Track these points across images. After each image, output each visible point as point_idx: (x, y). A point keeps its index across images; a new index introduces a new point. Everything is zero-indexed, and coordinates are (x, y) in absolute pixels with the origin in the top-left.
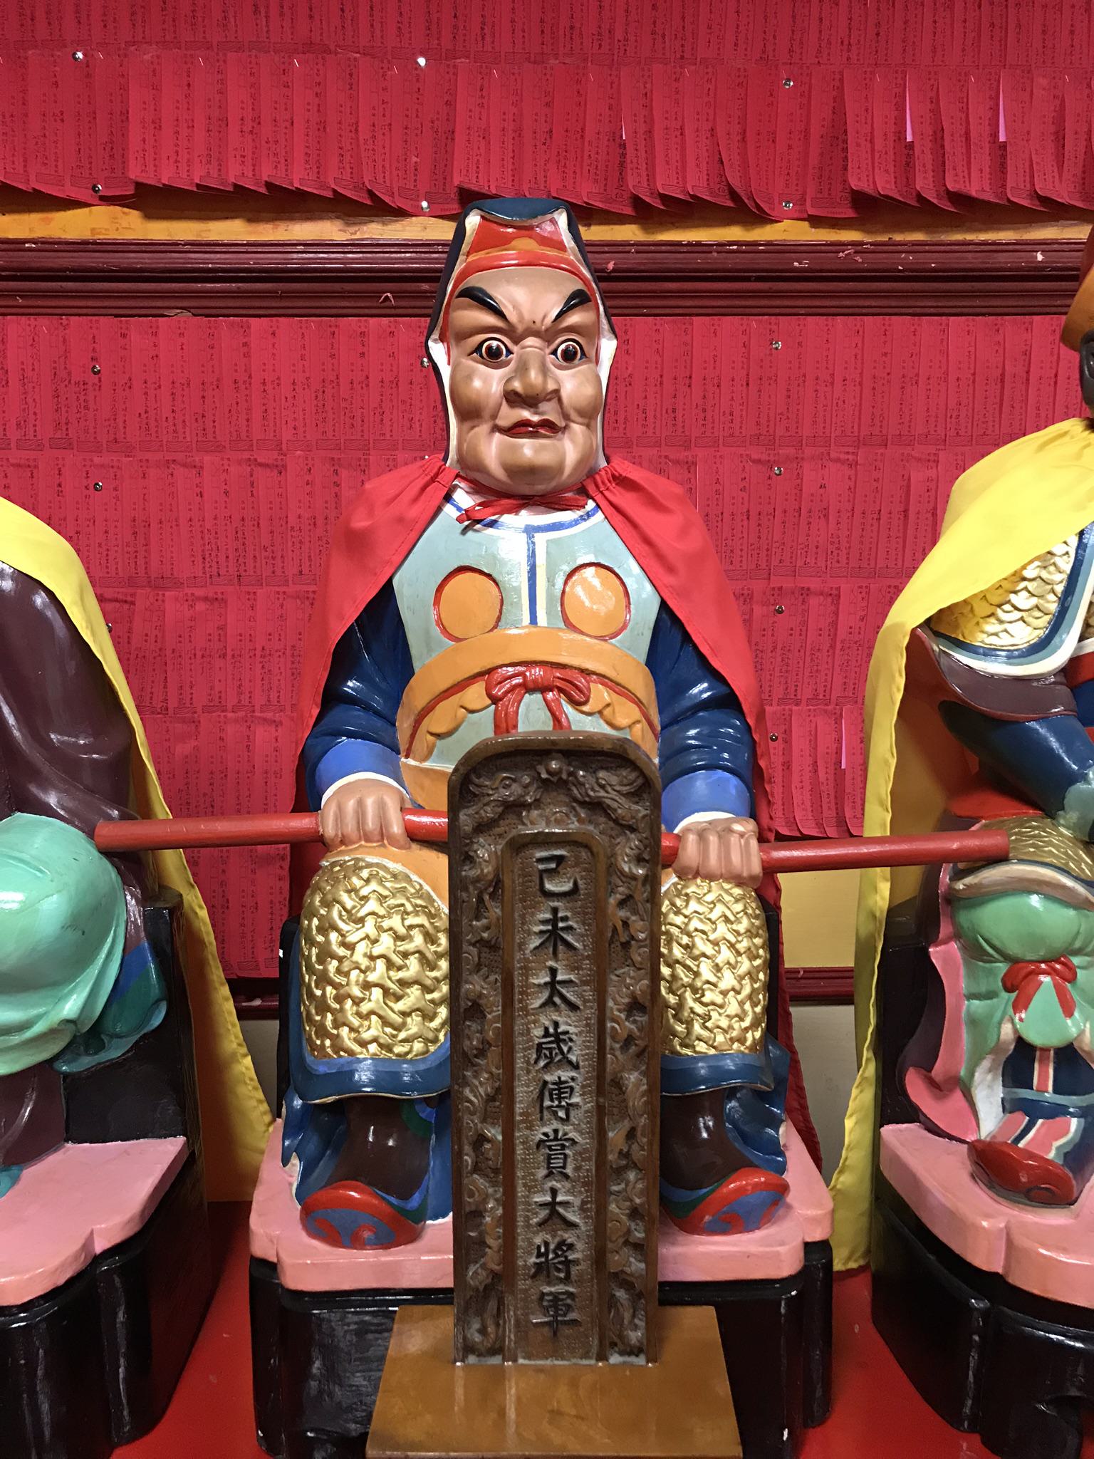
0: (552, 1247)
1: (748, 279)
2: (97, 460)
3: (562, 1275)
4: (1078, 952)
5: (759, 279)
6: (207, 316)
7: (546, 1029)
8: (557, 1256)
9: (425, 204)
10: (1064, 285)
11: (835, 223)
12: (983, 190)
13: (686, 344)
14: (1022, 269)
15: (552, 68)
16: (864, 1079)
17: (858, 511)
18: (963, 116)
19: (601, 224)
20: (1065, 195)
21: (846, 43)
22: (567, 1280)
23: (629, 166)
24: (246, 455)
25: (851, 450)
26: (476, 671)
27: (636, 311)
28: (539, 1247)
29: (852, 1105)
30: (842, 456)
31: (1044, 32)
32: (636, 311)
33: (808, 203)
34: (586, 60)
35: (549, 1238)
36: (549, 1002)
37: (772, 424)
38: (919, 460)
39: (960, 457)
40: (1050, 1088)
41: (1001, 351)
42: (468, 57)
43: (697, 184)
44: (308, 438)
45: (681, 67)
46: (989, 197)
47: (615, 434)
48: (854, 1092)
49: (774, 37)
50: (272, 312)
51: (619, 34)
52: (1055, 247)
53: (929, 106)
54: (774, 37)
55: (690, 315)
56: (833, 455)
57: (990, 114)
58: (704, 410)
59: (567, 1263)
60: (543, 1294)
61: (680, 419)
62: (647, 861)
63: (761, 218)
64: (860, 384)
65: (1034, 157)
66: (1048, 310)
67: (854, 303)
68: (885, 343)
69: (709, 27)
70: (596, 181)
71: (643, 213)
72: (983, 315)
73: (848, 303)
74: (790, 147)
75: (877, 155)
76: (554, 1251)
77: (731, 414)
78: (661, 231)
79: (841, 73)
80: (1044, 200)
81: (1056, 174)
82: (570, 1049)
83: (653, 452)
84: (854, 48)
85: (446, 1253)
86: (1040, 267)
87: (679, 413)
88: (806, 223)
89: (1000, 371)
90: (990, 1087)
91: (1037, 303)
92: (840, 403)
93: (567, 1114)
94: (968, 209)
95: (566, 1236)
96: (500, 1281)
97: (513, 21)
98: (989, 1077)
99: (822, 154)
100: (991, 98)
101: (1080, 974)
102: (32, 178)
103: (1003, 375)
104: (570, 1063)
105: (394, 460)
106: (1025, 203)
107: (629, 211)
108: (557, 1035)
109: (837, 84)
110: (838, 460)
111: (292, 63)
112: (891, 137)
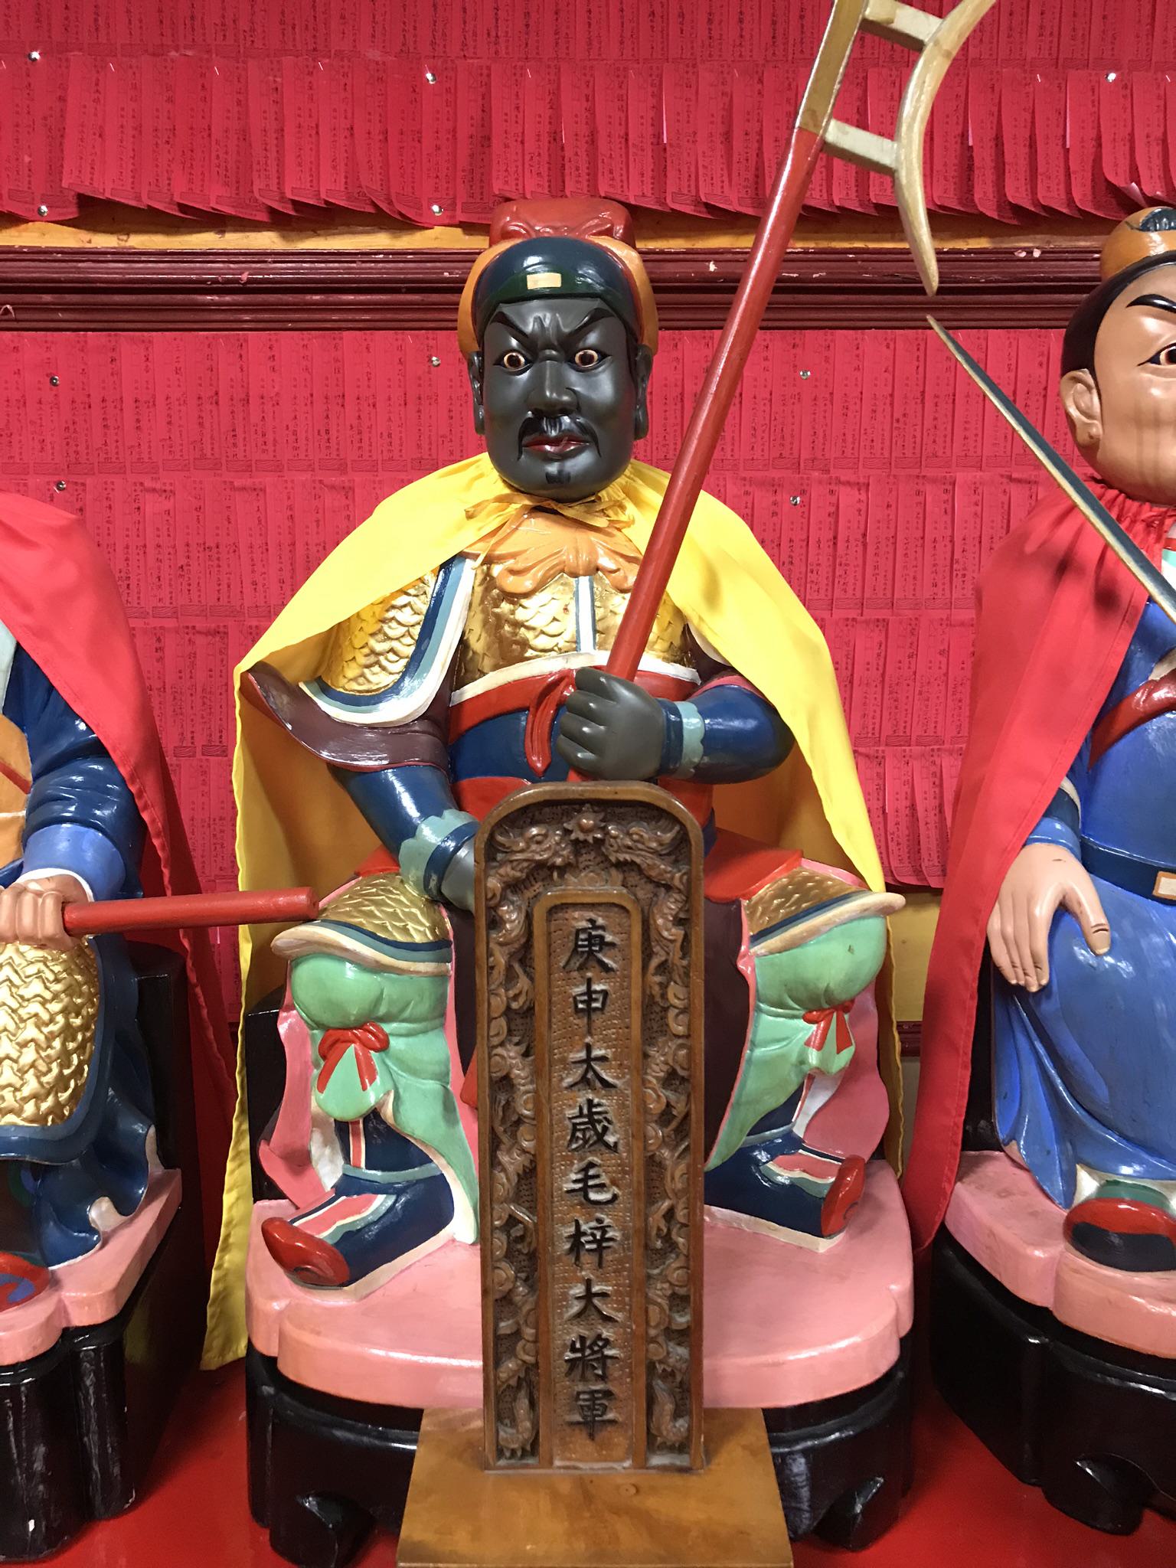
0: (588, 1343)
1: (397, 291)
2: (148, 484)
3: (600, 1372)
4: (388, 1018)
5: (410, 291)
6: (1041, 327)
7: (581, 1109)
8: (594, 1352)
9: (44, 208)
10: (716, 297)
12: (643, 195)
13: (337, 361)
14: (691, 280)
15: (172, 61)
16: (238, 1154)
18: (623, 115)
19: (236, 231)
20: (735, 202)
21: (493, 34)
22: (603, 1378)
23: (255, 167)
24: (916, 472)
26: (482, 718)
27: (280, 325)
28: (574, 1343)
29: (228, 1180)
31: (710, 21)
32: (280, 325)
33: (459, 207)
34: (209, 52)
35: (585, 1332)
36: (584, 1081)
37: (434, 447)
40: (363, 1164)
41: (679, 367)
42: (80, 50)
43: (331, 190)
45: (314, 60)
46: (854, 205)
47: (264, 457)
48: (229, 1166)
49: (415, 28)
51: (243, 25)
53: (585, 104)
54: (415, 28)
55: (339, 329)
57: (651, 114)
58: (360, 433)
60: (579, 1393)
61: (333, 441)
63: (406, 224)
65: (700, 159)
69: (343, 17)
70: (227, 184)
71: (278, 221)
74: (438, 148)
75: (527, 158)
76: (590, 1347)
77: (390, 436)
78: (301, 239)
79: (489, 68)
80: (1017, 210)
81: (726, 178)
82: (605, 1129)
83: (306, 477)
84: (502, 40)
86: (713, 278)
87: (333, 433)
88: (459, 230)
89: (679, 390)
90: (332, 1161)
93: (604, 1368)
96: (529, 1381)
97: (128, 11)
98: (327, 1151)
99: (472, 156)
101: (393, 1041)
102: (213, 199)
103: (682, 394)
104: (607, 1145)
105: (25, 485)
106: (689, 210)
107: (263, 217)
108: (591, 1114)
109: (485, 79)
111: (316, 67)
112: (545, 138)
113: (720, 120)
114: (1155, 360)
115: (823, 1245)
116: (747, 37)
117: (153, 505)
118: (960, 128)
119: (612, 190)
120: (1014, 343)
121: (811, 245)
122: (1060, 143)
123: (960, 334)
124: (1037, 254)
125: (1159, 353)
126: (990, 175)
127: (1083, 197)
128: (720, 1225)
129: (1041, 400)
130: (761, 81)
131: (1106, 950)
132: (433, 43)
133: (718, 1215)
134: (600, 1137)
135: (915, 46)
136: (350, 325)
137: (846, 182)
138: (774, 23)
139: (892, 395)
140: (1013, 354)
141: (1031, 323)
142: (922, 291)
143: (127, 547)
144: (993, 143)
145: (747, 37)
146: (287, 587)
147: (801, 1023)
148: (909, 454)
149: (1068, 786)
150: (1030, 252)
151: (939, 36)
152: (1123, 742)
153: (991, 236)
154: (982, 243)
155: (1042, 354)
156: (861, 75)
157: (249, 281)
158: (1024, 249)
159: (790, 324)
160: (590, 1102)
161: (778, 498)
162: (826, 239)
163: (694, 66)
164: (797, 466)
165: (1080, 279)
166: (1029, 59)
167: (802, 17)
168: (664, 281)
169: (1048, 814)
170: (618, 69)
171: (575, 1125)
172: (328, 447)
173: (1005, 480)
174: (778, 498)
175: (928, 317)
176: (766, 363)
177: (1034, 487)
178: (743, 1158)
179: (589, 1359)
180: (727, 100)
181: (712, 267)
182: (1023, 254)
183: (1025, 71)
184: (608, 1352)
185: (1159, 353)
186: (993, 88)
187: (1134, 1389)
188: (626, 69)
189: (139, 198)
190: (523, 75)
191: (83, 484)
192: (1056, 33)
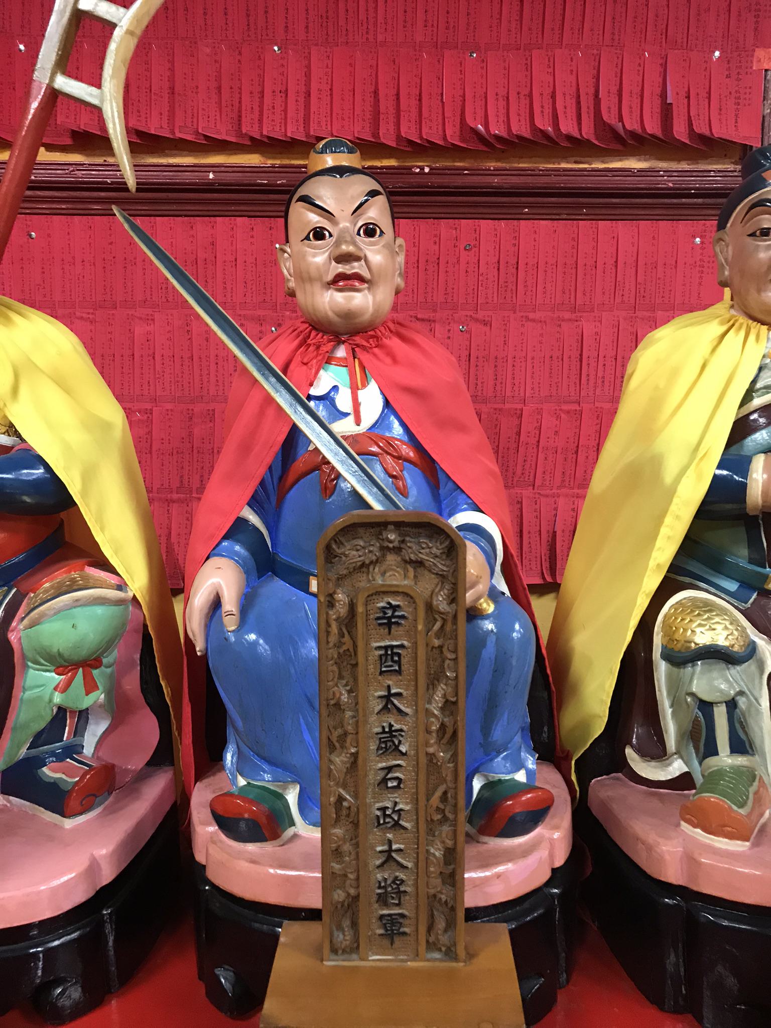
0: (389, 882)
3: (397, 902)
7: (383, 728)
11: (64, 149)
12: (161, 127)
17: (137, 356)
22: (398, 905)
25: (91, 311)
28: (380, 882)
30: (85, 315)
31: (205, 14)
36: (385, 708)
38: (141, 318)
39: (170, 317)
44: (435, 300)
49: (10, 17)
50: (509, 216)
52: (223, 169)
56: (78, 314)
57: (168, 73)
59: (400, 893)
62: (473, 914)
64: (94, 264)
66: (227, 213)
67: (197, 208)
68: (110, 235)
72: (181, 216)
73: (406, 210)
76: (390, 885)
80: (702, 138)
81: (218, 118)
85: (470, 879)
86: (211, 183)
91: (643, 213)
92: (81, 277)
94: (578, 146)
95: (397, 874)
96: (352, 905)
100: (661, 65)
104: (401, 752)
107: (69, 141)
108: (391, 731)
110: (82, 318)
113: (167, 79)
114: (307, 238)
115: (69, 824)
116: (230, 25)
117: (140, 330)
118: (373, 87)
119: (138, 124)
120: (417, 228)
121: (278, 162)
122: (440, 98)
123: (138, 221)
124: (427, 170)
125: (309, 234)
126: (392, 119)
127: (588, 132)
128: (15, 810)
129: (436, 267)
130: (240, 53)
131: (233, 628)
132: (22, 26)
133: (13, 802)
134: (397, 747)
135: (113, 26)
136: (404, 215)
137: (297, 121)
138: (248, 15)
139: (418, 261)
140: (417, 236)
141: (440, 215)
142: (127, 190)
143: (142, 356)
144: (395, 97)
145: (230, 25)
146: (60, 312)
147: (53, 674)
148: (470, 301)
149: (253, 518)
150: (422, 169)
151: (125, 20)
152: (292, 492)
153: (397, 158)
154: (392, 162)
155: (435, 236)
156: (306, 51)
157: (112, 183)
158: (418, 167)
159: (268, 214)
160: (391, 726)
161: (263, 328)
162: (288, 158)
163: (196, 43)
164: (274, 308)
165: (456, 187)
166: (418, 42)
167: (266, 12)
168: (481, 188)
169: (225, 537)
170: (145, 44)
171: (380, 739)
172: (265, 293)
173: (413, 319)
174: (263, 328)
175: (114, 207)
176: (252, 240)
177: (433, 325)
178: (31, 764)
179: (390, 893)
180: (218, 65)
181: (211, 176)
182: (418, 170)
183: (415, 50)
184: (402, 888)
185: (309, 234)
186: (394, 61)
187: (754, 926)
188: (149, 44)
189: (174, 133)
190: (150, 49)
191: (113, 314)
192: (435, 25)
